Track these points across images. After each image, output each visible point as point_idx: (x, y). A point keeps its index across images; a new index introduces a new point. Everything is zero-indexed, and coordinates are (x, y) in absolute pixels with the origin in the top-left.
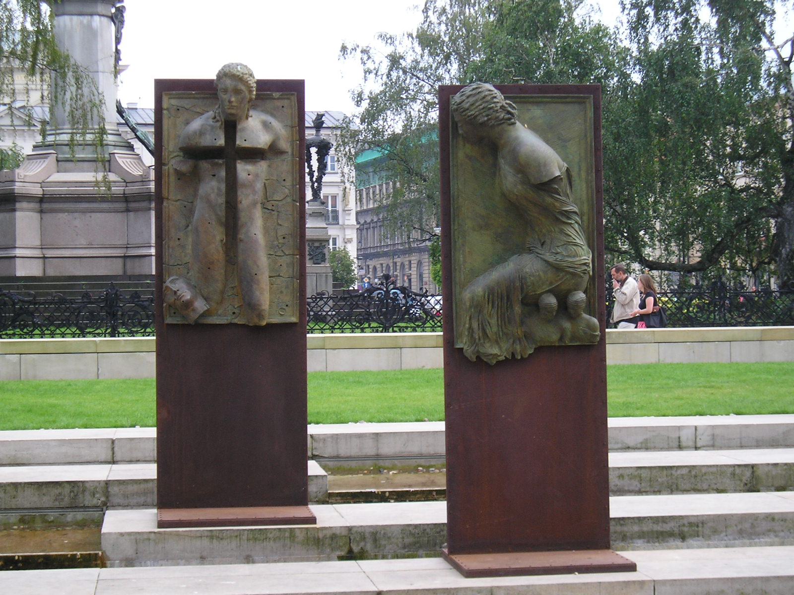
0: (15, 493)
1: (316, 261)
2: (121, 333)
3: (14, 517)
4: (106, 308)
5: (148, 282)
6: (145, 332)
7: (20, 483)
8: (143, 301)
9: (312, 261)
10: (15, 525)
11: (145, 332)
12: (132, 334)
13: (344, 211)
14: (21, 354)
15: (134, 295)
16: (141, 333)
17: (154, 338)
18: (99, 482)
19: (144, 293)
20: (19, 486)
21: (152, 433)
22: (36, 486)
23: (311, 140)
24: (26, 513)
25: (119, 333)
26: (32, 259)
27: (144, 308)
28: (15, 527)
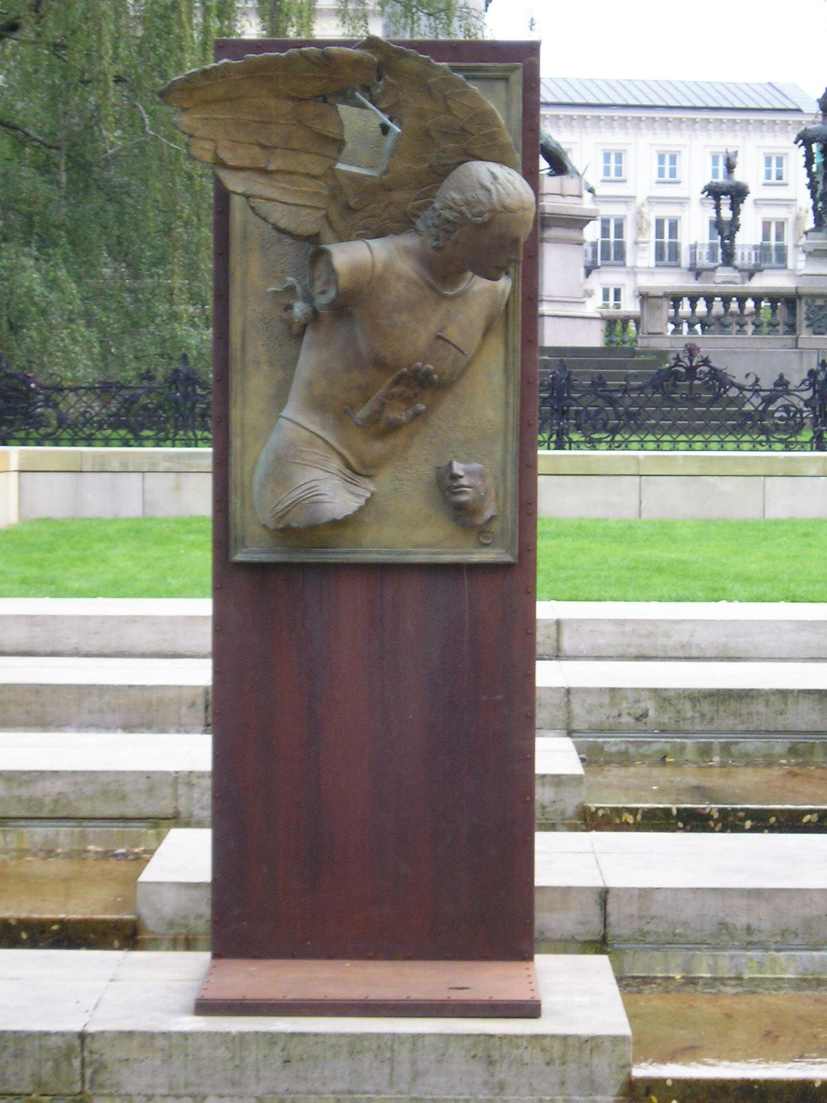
0: (783, 706)
1: (818, 330)
2: (575, 442)
3: (780, 745)
4: (551, 401)
5: (546, 358)
6: (612, 441)
7: (792, 691)
8: (611, 391)
9: (811, 329)
10: (781, 757)
11: (612, 441)
12: (593, 444)
13: (636, 243)
14: (641, 476)
15: (597, 380)
16: (607, 442)
17: (210, 450)
18: (196, 687)
19: (613, 377)
20: (790, 695)
21: (204, 607)
22: (816, 696)
23: (816, 130)
24: (797, 739)
25: (571, 442)
26: (566, 319)
27: (612, 402)
28: (784, 761)
